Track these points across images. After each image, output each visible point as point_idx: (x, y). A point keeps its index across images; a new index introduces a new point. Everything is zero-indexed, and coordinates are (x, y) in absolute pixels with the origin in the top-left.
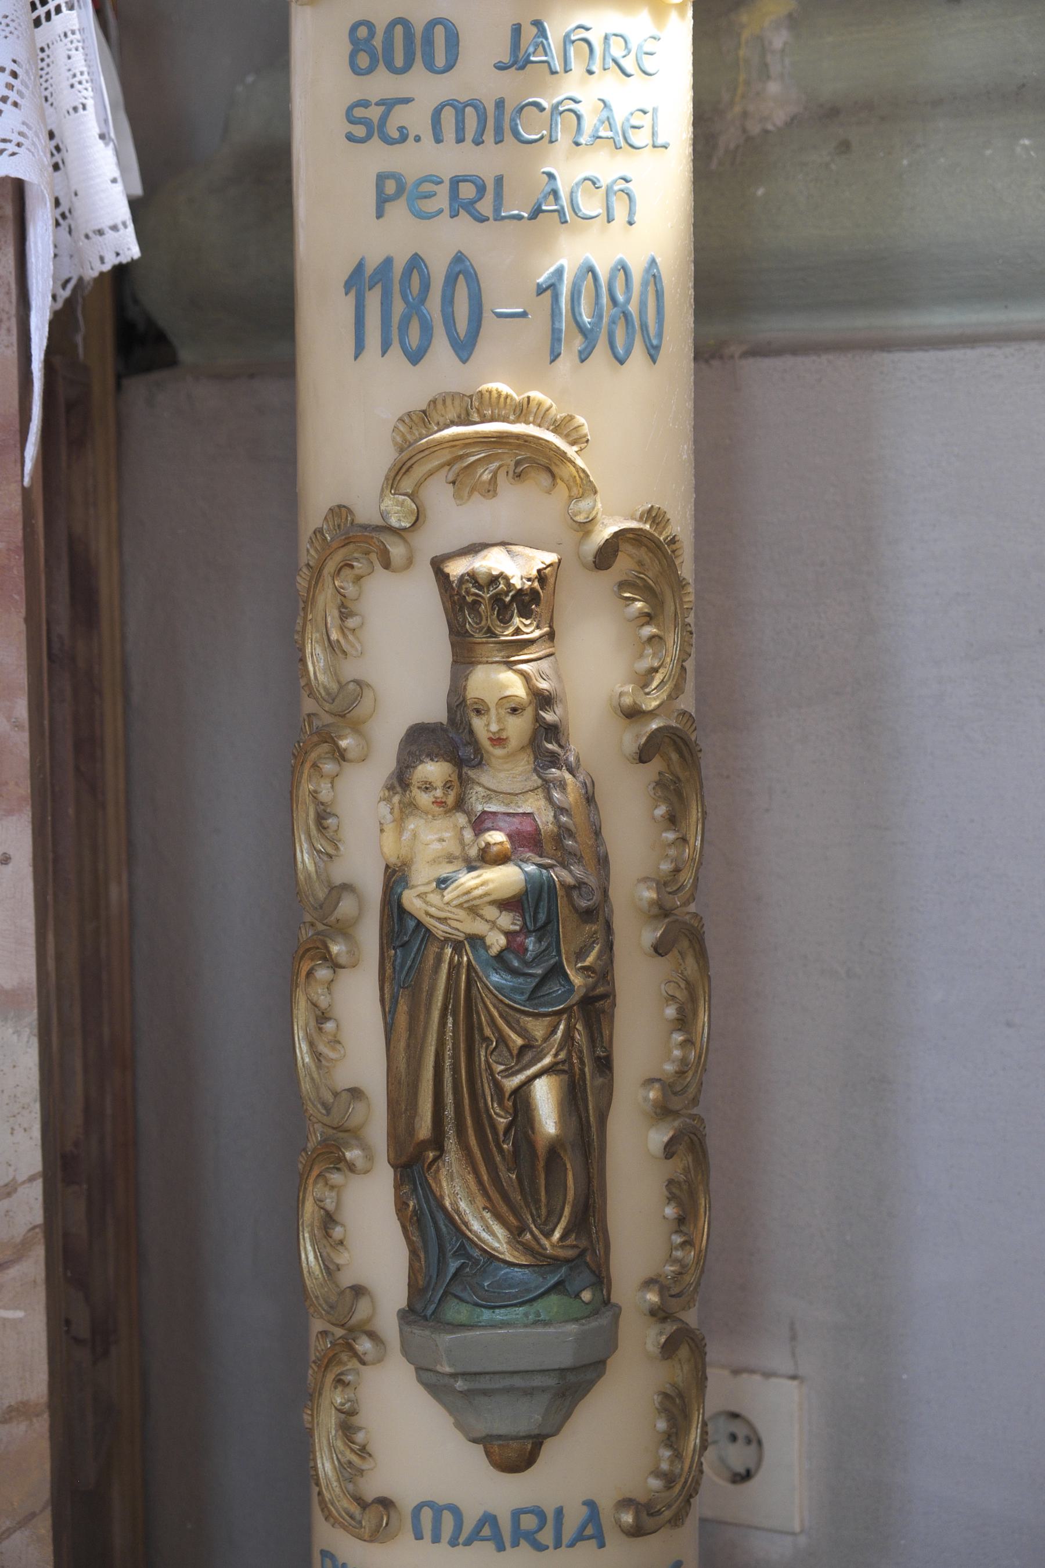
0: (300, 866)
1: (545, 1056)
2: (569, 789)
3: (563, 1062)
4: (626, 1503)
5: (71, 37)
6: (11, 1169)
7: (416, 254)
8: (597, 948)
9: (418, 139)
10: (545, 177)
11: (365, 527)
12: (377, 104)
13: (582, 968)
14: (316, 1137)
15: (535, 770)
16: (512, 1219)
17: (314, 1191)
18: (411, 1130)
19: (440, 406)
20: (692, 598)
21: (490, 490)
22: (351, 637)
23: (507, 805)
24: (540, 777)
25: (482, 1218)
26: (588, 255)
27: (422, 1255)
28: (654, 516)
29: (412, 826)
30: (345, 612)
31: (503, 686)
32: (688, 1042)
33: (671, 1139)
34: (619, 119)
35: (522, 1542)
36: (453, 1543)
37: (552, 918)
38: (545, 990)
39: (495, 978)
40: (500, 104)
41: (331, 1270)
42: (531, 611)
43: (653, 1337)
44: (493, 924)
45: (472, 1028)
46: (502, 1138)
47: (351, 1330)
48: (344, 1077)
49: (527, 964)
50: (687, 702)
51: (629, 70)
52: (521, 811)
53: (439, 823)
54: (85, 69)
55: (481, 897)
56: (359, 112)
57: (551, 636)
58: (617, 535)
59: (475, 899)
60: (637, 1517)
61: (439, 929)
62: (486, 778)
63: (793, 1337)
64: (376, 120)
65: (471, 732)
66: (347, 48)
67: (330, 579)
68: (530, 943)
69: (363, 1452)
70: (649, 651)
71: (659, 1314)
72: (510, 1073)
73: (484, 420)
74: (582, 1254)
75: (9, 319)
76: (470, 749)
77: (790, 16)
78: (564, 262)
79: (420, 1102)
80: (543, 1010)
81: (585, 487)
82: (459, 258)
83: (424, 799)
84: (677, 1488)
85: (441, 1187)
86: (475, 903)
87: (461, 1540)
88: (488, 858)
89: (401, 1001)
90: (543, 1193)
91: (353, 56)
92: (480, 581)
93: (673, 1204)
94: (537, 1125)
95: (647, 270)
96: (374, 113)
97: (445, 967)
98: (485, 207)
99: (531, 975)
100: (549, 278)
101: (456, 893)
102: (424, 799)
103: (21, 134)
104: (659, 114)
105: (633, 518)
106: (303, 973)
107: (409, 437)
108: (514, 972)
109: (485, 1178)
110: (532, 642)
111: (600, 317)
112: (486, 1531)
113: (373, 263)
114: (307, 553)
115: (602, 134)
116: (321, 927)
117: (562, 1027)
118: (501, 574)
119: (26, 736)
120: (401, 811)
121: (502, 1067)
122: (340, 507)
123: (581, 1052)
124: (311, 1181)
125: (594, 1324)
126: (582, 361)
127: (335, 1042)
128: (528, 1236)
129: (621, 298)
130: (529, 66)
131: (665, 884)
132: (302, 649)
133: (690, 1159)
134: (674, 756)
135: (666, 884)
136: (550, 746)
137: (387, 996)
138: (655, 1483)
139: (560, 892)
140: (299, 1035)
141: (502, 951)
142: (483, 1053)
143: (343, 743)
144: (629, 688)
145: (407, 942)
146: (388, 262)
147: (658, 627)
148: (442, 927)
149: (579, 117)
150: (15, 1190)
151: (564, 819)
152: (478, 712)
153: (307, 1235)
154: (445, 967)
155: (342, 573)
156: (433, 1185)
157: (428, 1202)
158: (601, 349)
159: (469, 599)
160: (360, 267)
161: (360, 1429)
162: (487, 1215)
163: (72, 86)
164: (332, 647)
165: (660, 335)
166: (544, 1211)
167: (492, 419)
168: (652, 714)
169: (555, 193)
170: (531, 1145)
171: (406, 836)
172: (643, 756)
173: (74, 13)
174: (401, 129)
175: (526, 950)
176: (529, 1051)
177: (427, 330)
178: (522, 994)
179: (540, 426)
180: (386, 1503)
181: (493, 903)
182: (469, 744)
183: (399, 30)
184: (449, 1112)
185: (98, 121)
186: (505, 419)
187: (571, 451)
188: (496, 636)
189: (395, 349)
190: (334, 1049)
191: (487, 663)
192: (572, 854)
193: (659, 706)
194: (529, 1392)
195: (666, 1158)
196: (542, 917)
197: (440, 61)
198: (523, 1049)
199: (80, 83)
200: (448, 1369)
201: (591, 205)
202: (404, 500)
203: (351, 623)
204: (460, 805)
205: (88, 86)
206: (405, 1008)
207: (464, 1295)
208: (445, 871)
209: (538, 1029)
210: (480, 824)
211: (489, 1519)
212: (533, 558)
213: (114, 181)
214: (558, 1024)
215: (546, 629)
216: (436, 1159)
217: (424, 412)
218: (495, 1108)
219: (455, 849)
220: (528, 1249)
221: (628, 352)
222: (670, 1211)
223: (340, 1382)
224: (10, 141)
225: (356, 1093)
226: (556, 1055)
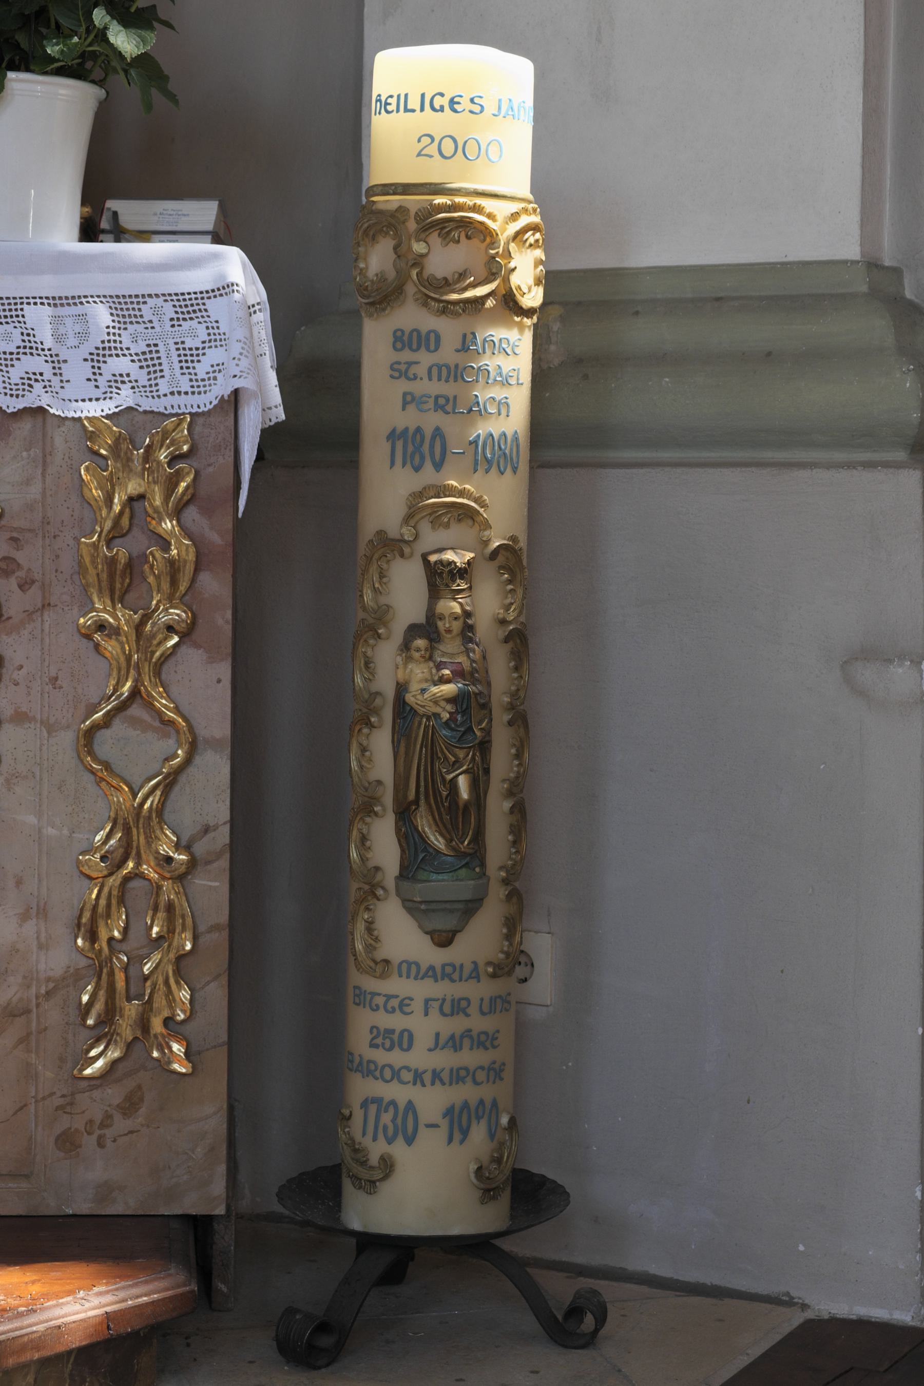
0: (356, 684)
1: (464, 766)
2: (477, 652)
3: (471, 768)
4: (489, 963)
5: (260, 324)
6: (216, 819)
7: (419, 427)
8: (486, 721)
9: (421, 379)
10: (474, 397)
11: (393, 540)
12: (404, 363)
13: (481, 728)
14: (359, 802)
15: (463, 644)
16: (448, 836)
17: (358, 825)
18: (406, 796)
19: (427, 489)
20: (527, 574)
21: (447, 526)
22: (384, 586)
23: (451, 658)
24: (465, 647)
25: (435, 835)
26: (491, 429)
27: (407, 852)
28: (514, 539)
29: (410, 667)
30: (382, 576)
31: (452, 608)
32: (520, 765)
33: (513, 805)
34: (504, 373)
35: (446, 978)
36: (416, 978)
37: (469, 707)
38: (464, 738)
39: (444, 732)
40: (457, 366)
41: (363, 859)
42: (464, 577)
43: (502, 892)
44: (444, 709)
45: (433, 754)
46: (444, 800)
47: (373, 886)
48: (373, 776)
49: (458, 726)
50: (522, 619)
51: (509, 353)
52: (456, 661)
53: (422, 665)
54: (265, 338)
55: (440, 697)
56: (396, 366)
57: (470, 588)
58: (499, 546)
59: (437, 698)
60: (494, 969)
61: (421, 710)
62: (442, 647)
63: (549, 915)
64: (403, 370)
65: (436, 627)
66: (392, 340)
67: (375, 561)
68: (459, 717)
69: (377, 939)
70: (510, 596)
71: (506, 882)
72: (449, 772)
73: (446, 496)
74: (476, 852)
75: (231, 445)
76: (436, 635)
77: (561, 316)
78: (480, 431)
79: (410, 784)
80: (464, 746)
81: (487, 525)
82: (437, 429)
83: (416, 655)
84: (511, 959)
85: (417, 821)
86: (437, 699)
87: (419, 977)
88: (443, 681)
89: (402, 742)
90: (461, 825)
91: (394, 343)
92: (445, 564)
93: (512, 835)
94: (460, 794)
95: (514, 436)
96: (403, 367)
97: (423, 726)
98: (449, 408)
99: (459, 731)
100: (474, 438)
101: (429, 695)
102: (416, 655)
103: (249, 369)
104: (520, 371)
105: (505, 539)
106: (356, 731)
107: (413, 502)
108: (452, 729)
109: (437, 817)
110: (464, 590)
111: (495, 455)
112: (430, 973)
113: (400, 428)
114: (362, 548)
115: (498, 379)
116: (365, 710)
117: (471, 753)
118: (453, 561)
119: (230, 627)
120: (406, 661)
121: (445, 770)
122: (381, 531)
123: (478, 765)
124: (356, 821)
125: (481, 882)
126: (487, 473)
127: (370, 760)
128: (454, 843)
129: (503, 447)
130: (469, 351)
131: (513, 696)
132: (361, 591)
133: (519, 816)
134: (518, 641)
135: (514, 695)
136: (469, 634)
137: (396, 739)
138: (501, 956)
139: (473, 696)
140: (353, 757)
141: (448, 720)
142: (437, 764)
143: (380, 631)
144: (502, 611)
145: (406, 716)
146: (407, 429)
147: (513, 585)
148: (422, 709)
149: (489, 372)
150: (218, 828)
151: (474, 665)
152: (440, 619)
153: (353, 846)
154: (423, 726)
155: (382, 559)
156: (414, 821)
157: (410, 828)
158: (494, 469)
159: (439, 571)
160: (394, 430)
161: (375, 929)
162: (437, 834)
163: (260, 345)
164: (375, 590)
165: (518, 463)
166: (460, 833)
167: (449, 496)
168: (510, 622)
169: (478, 403)
170: (457, 804)
171: (408, 670)
172: (506, 640)
173: (262, 314)
174: (414, 374)
175: (457, 720)
176: (457, 763)
177: (423, 458)
178: (455, 739)
179: (469, 499)
180: (387, 962)
181: (444, 700)
182: (434, 632)
183: (415, 334)
184: (422, 789)
185: (270, 360)
186: (454, 496)
187: (481, 510)
188: (450, 587)
189: (408, 465)
190: (369, 764)
191: (445, 598)
192: (478, 680)
193: (514, 619)
194: (451, 911)
195: (510, 814)
196: (464, 706)
197: (432, 347)
198: (454, 763)
199: (264, 344)
200: (419, 899)
201: (492, 410)
202: (410, 530)
203: (385, 580)
204: (431, 658)
205: (267, 345)
206: (404, 745)
207: (426, 868)
208: (424, 685)
209: (461, 754)
210: (439, 666)
211: (432, 968)
212: (465, 555)
213: (276, 386)
214: (470, 753)
215: (469, 585)
216: (416, 809)
217: (420, 492)
218: (441, 788)
219: (427, 676)
220: (454, 849)
221: (505, 470)
222: (510, 838)
223: (367, 909)
224: (244, 372)
225: (379, 783)
226: (468, 765)
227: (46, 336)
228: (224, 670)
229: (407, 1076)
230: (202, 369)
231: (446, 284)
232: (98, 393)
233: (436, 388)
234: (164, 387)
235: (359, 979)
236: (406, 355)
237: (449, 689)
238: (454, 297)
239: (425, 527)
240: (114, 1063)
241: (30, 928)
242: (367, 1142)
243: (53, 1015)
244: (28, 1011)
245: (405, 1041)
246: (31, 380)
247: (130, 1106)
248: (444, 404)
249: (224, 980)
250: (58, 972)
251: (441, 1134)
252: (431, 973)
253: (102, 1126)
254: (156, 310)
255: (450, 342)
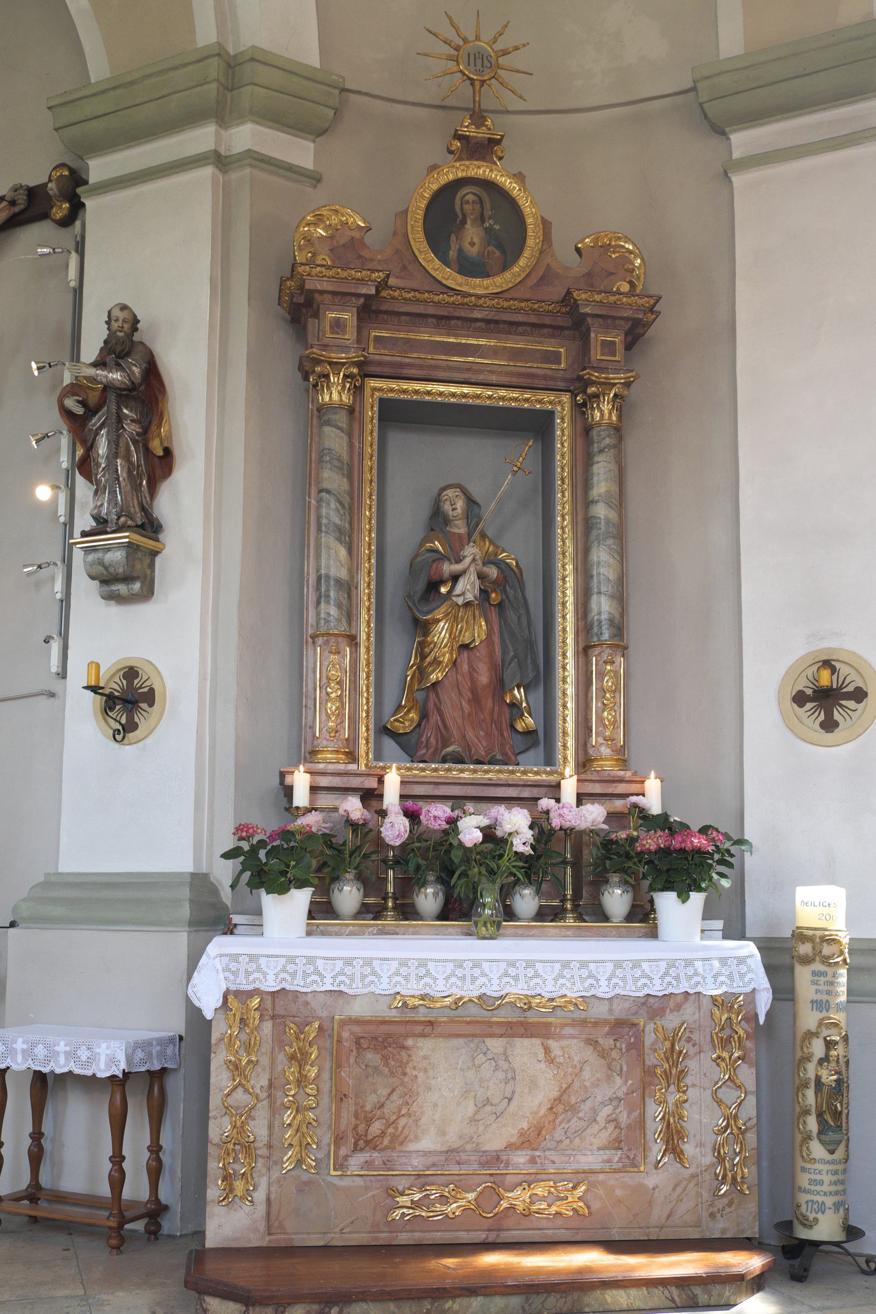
88: (832, 1075)
164: (807, 1047)
227: (700, 970)
228: (753, 1070)
229: (822, 1193)
230: (746, 980)
231: (829, 957)
232: (716, 987)
233: (826, 988)
234: (735, 985)
235: (800, 1163)
236: (816, 978)
237: (835, 1077)
238: (831, 961)
239: (824, 1029)
240: (727, 1190)
241: (698, 1150)
242: (808, 1213)
243: (707, 1176)
244: (698, 1176)
245: (821, 1183)
246: (697, 984)
247: (730, 1204)
248: (828, 993)
249: (756, 1165)
250: (708, 1163)
251: (832, 1211)
252: (828, 1162)
253: (722, 1210)
254: (732, 962)
255: (830, 974)
